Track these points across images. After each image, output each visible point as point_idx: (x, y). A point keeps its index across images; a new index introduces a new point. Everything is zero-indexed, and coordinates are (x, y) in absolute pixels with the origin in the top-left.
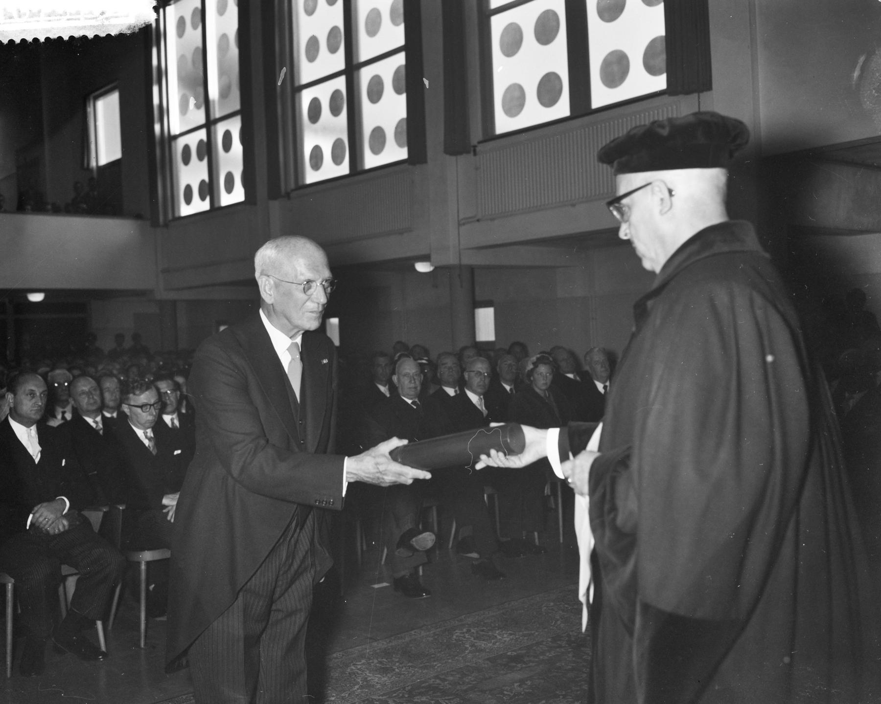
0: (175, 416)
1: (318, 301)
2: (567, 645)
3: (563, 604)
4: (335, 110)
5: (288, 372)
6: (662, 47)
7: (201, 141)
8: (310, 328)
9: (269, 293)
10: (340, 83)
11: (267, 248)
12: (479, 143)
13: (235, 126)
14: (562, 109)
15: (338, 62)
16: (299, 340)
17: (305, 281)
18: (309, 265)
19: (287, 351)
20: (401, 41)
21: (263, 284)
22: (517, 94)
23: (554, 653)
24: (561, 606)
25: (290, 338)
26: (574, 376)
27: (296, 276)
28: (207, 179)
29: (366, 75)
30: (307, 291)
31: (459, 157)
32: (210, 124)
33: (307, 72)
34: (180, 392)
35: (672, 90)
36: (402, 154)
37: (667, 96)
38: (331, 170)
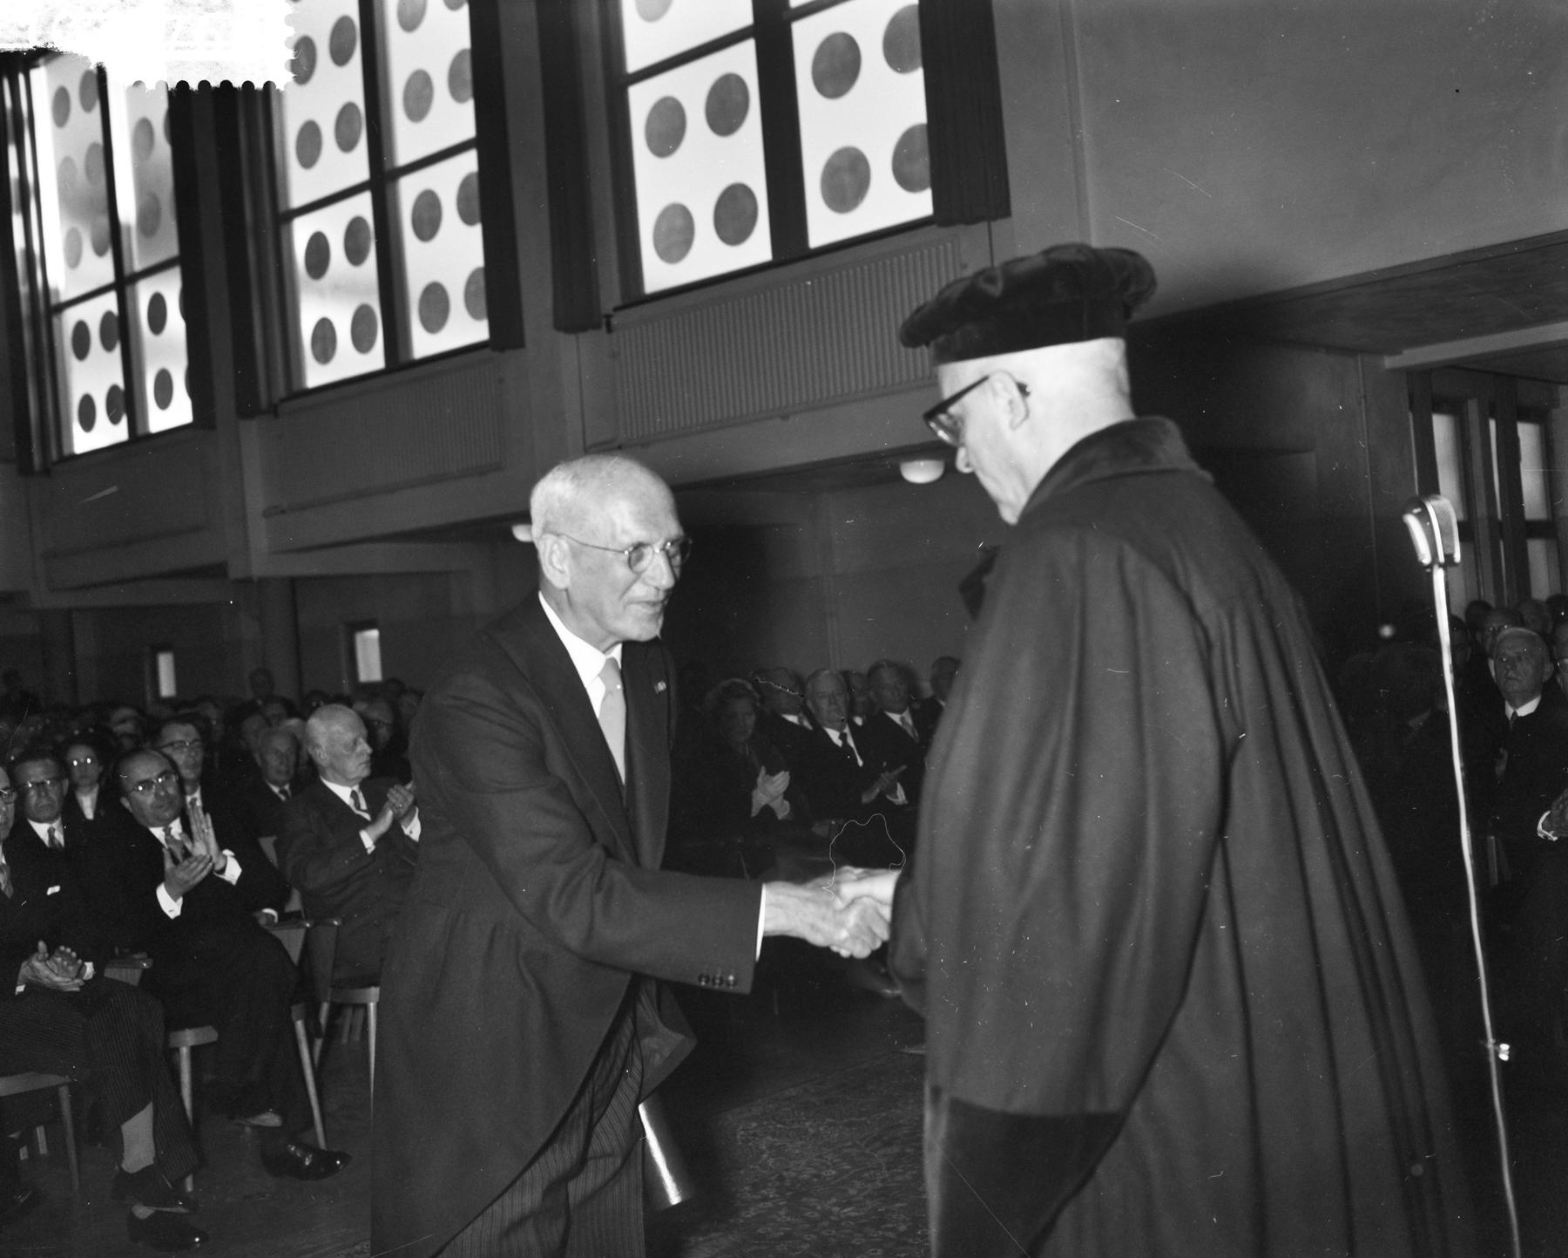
0: (56, 824)
1: (655, 584)
2: (777, 1196)
3: (774, 1123)
4: (355, 255)
5: (601, 713)
6: (922, 143)
7: (108, 315)
8: (640, 635)
9: (559, 567)
10: (362, 206)
11: (555, 479)
12: (617, 309)
13: (170, 287)
14: (758, 248)
15: (356, 166)
16: (617, 653)
17: (633, 545)
18: (639, 513)
19: (599, 679)
20: (468, 131)
21: (548, 550)
22: (679, 222)
23: (755, 1211)
24: (770, 1127)
25: (604, 652)
26: (800, 719)
27: (614, 537)
28: (121, 384)
29: (409, 190)
30: (635, 564)
31: (581, 335)
32: (123, 283)
33: (301, 185)
34: (70, 780)
35: (945, 214)
36: (478, 331)
37: (934, 227)
38: (350, 362)
